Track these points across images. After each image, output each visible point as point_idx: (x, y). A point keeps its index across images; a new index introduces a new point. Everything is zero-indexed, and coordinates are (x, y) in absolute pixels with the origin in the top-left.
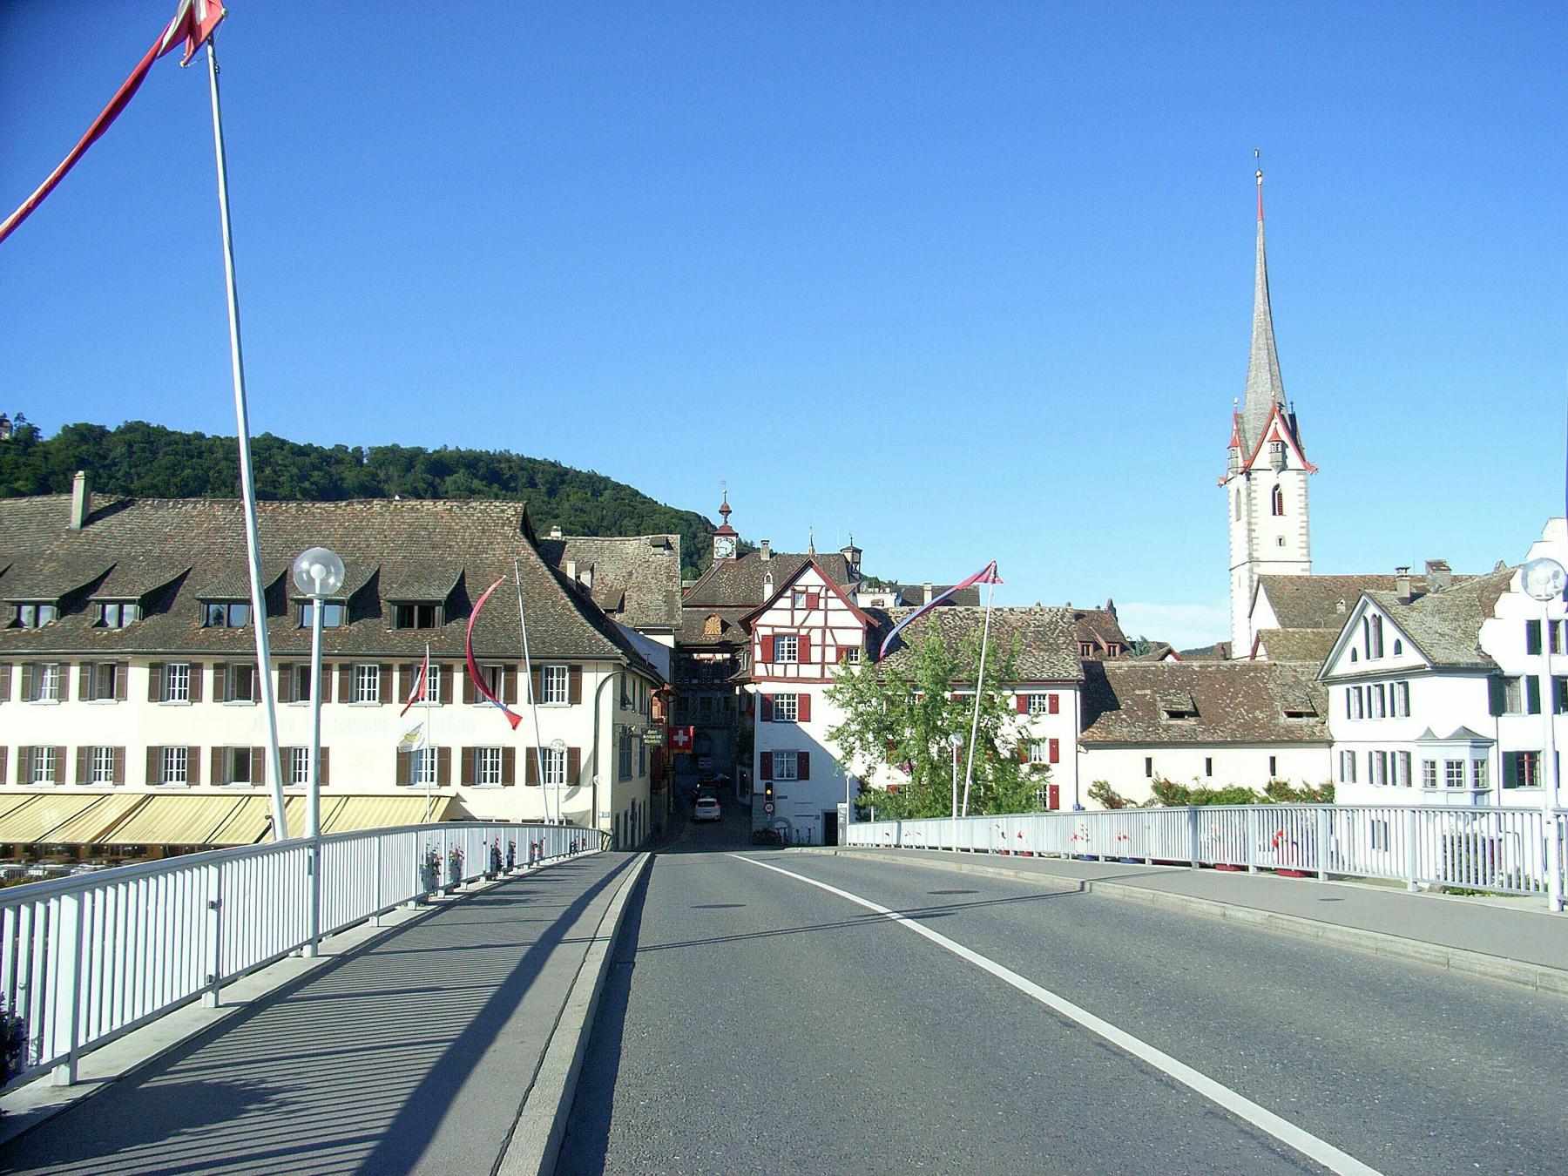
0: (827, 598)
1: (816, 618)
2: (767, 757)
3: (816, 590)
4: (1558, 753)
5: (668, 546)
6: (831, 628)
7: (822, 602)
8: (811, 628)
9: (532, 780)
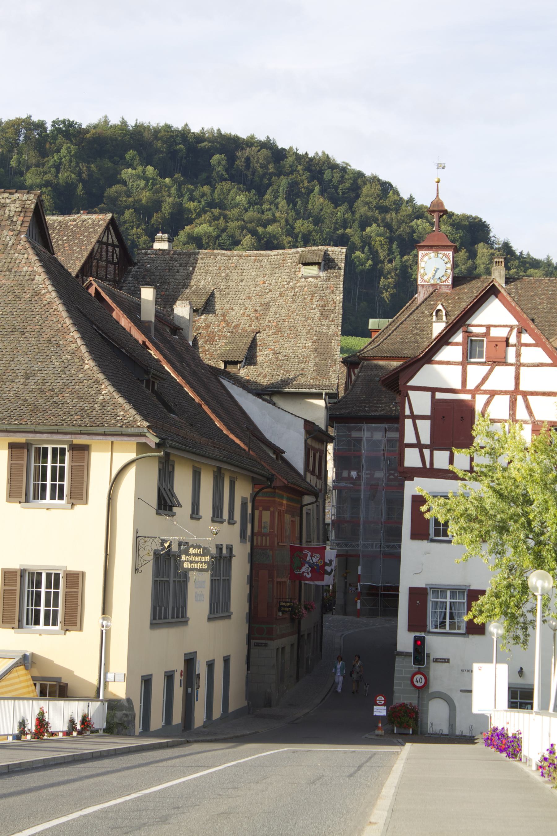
0: (520, 345)
1: (502, 378)
2: (418, 595)
3: (501, 333)
4: (104, 613)
5: (327, 263)
6: (525, 394)
7: (511, 351)
8: (493, 394)
9: (47, 623)
